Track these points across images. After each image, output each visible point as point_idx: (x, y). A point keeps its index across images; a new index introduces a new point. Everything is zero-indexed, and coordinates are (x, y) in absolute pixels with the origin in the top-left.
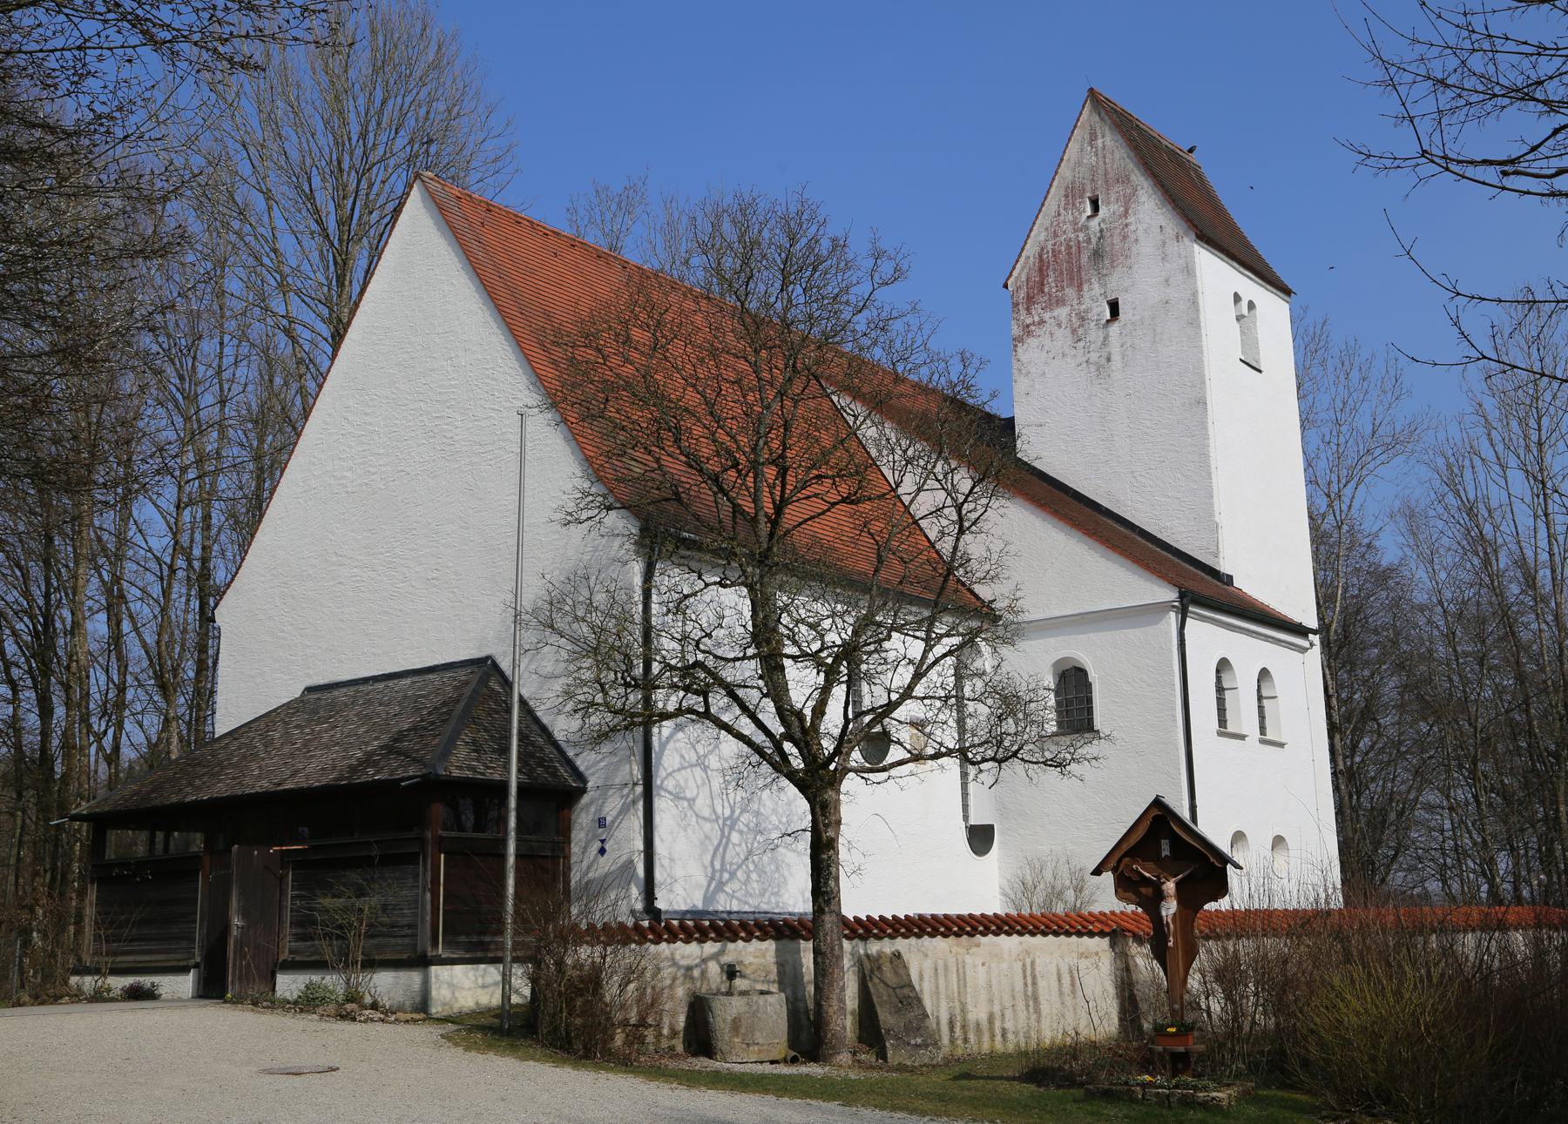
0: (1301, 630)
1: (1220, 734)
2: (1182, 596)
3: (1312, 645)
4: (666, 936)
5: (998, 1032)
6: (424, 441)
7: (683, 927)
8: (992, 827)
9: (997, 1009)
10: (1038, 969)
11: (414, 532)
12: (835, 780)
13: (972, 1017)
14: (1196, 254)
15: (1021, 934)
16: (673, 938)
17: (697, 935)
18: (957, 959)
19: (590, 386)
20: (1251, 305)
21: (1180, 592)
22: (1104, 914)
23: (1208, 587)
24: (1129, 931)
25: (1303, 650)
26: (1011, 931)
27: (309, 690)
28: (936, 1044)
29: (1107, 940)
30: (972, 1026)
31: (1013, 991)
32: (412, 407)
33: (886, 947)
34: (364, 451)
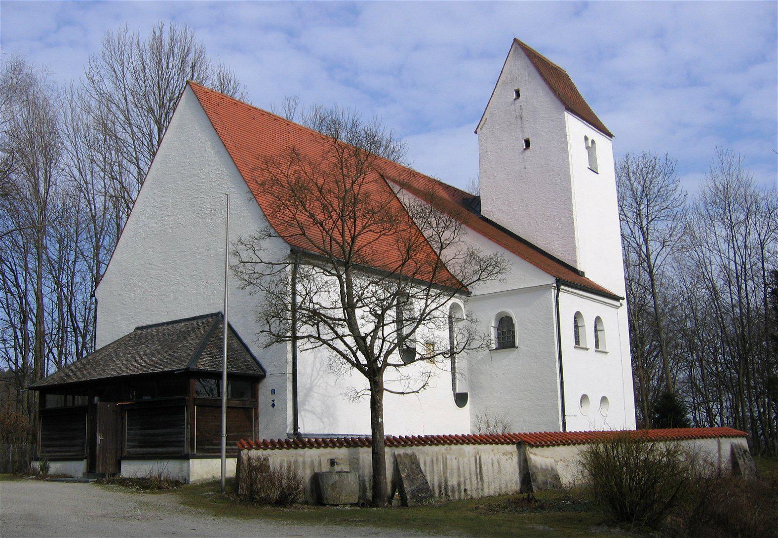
0: (617, 298)
1: (575, 347)
2: (558, 281)
3: (621, 305)
4: (278, 446)
5: (462, 490)
6: (190, 209)
7: (316, 440)
8: (466, 394)
9: (462, 479)
10: (482, 460)
11: (185, 253)
12: (380, 371)
13: (450, 483)
14: (566, 116)
15: (474, 444)
16: (304, 446)
17: (316, 445)
18: (443, 456)
19: (113, 152)
20: (593, 142)
21: (556, 279)
22: (576, 432)
23: (571, 277)
24: (527, 442)
25: (617, 307)
26: (469, 443)
27: (138, 329)
28: (432, 496)
29: (515, 445)
30: (450, 489)
31: (470, 471)
32: (184, 192)
33: (409, 450)
34: (162, 214)
